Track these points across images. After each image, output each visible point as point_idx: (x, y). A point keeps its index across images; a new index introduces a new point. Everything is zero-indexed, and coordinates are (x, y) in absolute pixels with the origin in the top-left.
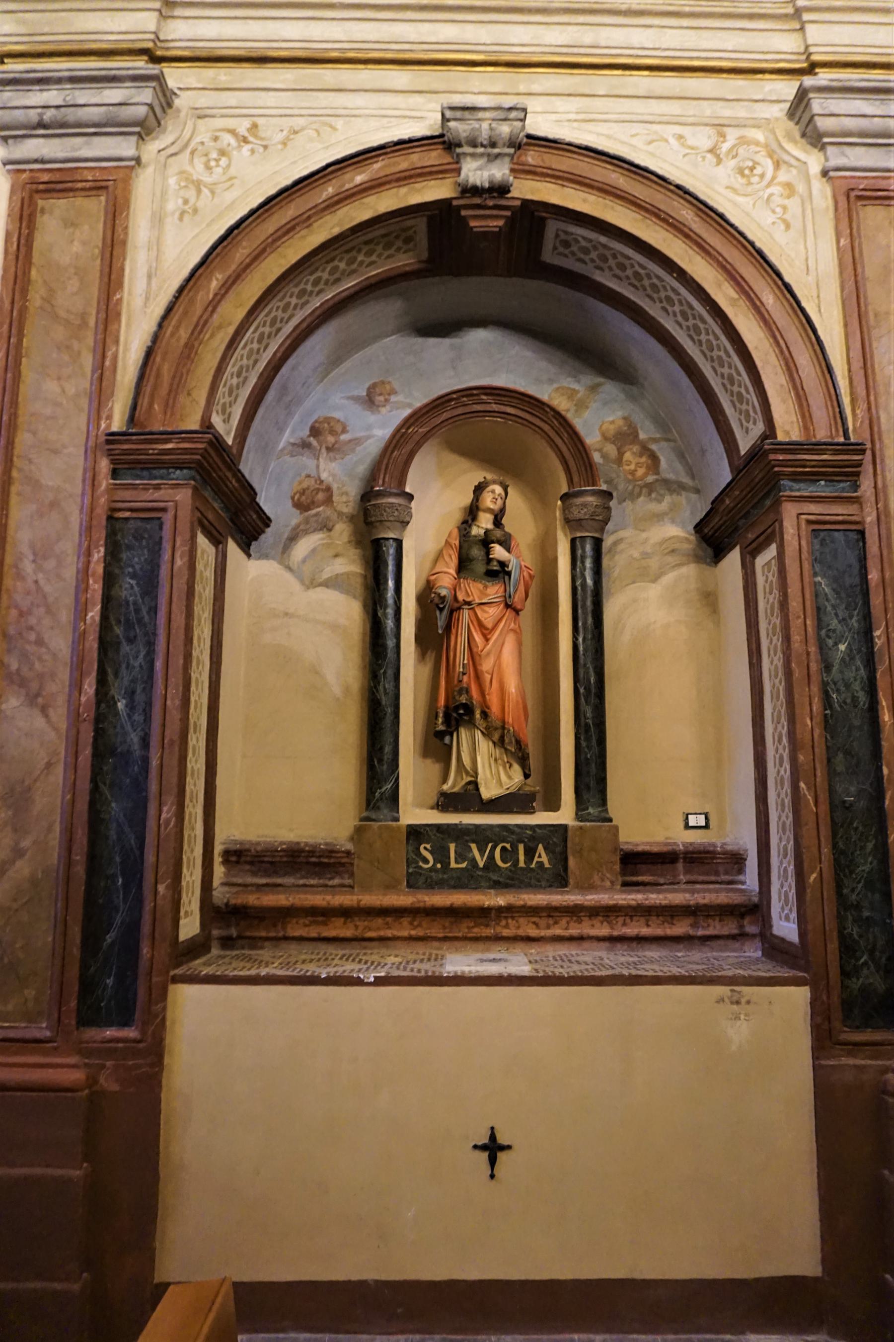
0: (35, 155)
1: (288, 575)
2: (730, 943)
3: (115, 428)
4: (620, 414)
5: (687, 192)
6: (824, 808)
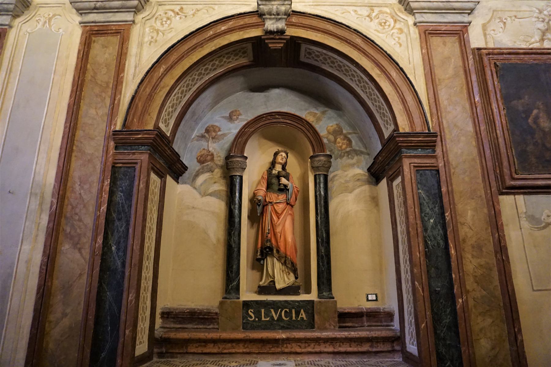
0: (92, 20)
1: (194, 191)
2: (388, 355)
3: (118, 128)
4: (335, 123)
5: (358, 32)
6: (427, 294)
